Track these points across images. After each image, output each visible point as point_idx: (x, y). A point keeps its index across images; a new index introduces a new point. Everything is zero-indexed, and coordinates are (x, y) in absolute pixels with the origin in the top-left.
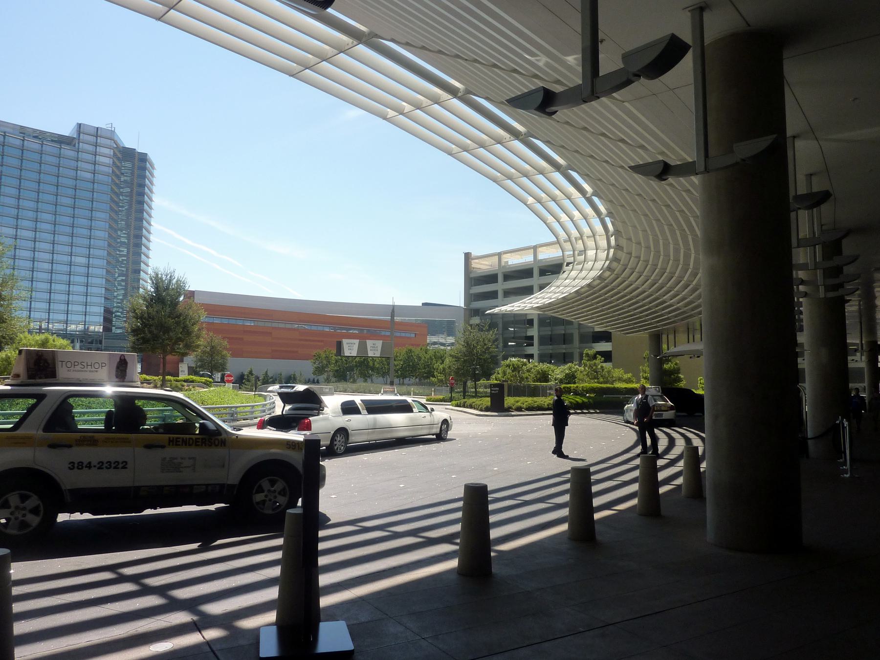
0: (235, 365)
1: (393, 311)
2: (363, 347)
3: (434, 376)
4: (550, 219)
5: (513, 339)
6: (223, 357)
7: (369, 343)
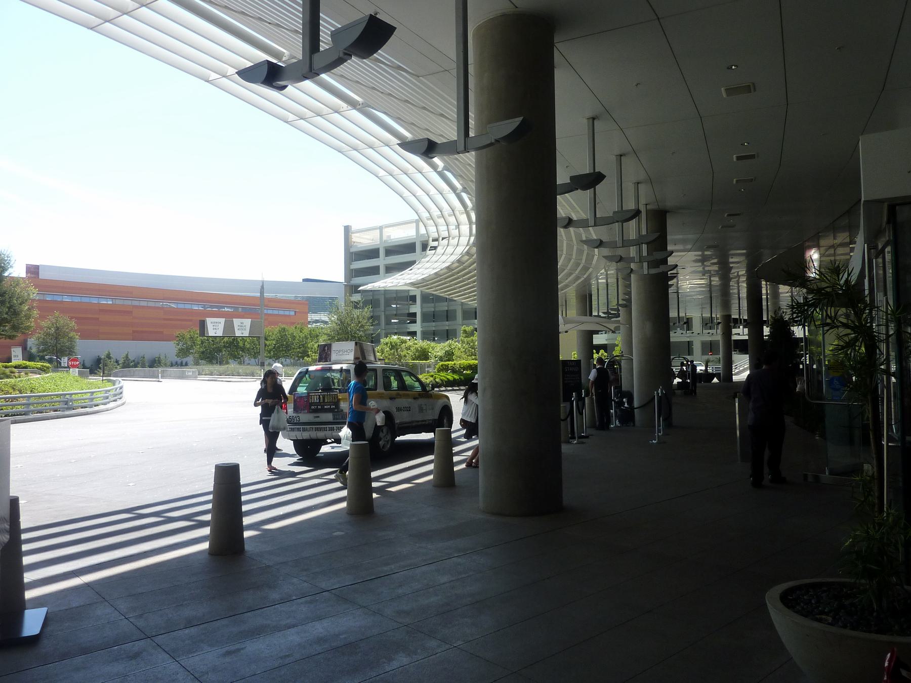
0: (86, 348)
1: (262, 287)
2: (229, 327)
3: (308, 356)
4: (406, 193)
5: (396, 316)
6: (71, 339)
7: (237, 322)
